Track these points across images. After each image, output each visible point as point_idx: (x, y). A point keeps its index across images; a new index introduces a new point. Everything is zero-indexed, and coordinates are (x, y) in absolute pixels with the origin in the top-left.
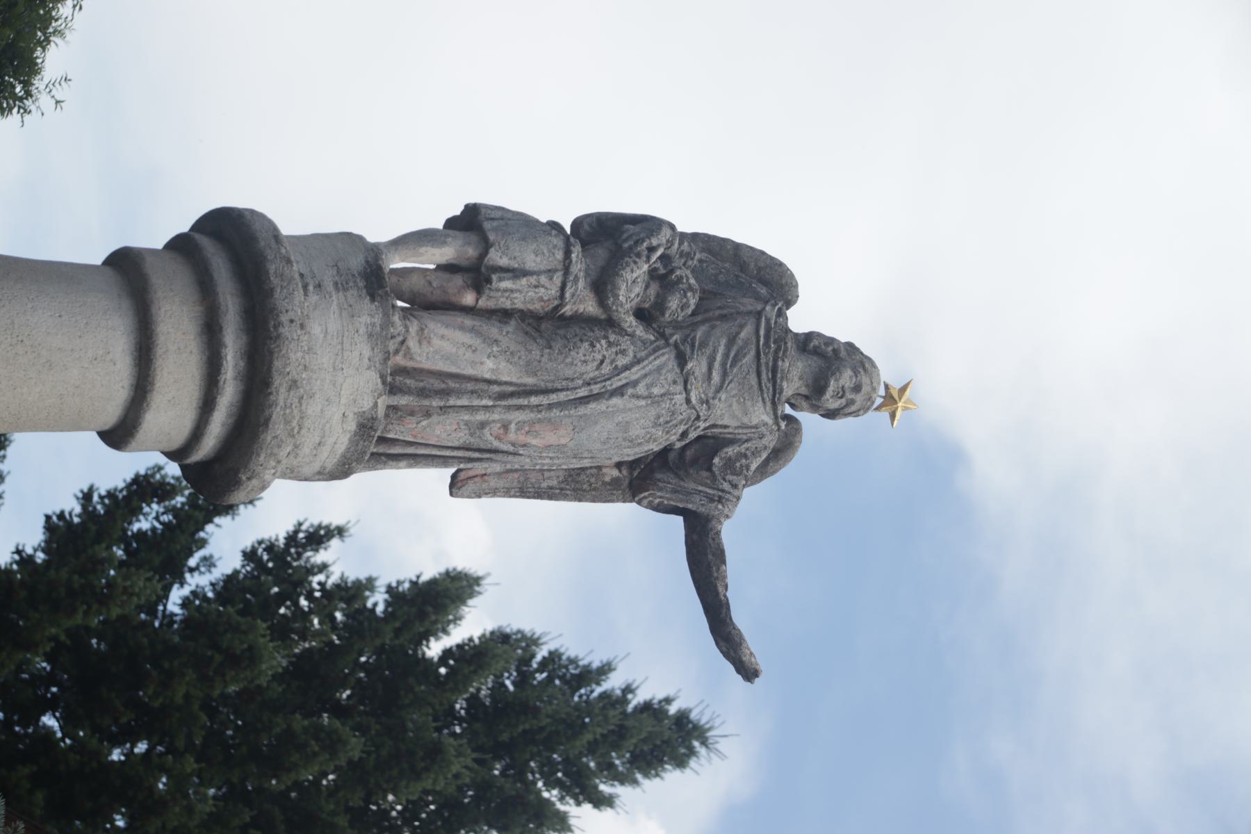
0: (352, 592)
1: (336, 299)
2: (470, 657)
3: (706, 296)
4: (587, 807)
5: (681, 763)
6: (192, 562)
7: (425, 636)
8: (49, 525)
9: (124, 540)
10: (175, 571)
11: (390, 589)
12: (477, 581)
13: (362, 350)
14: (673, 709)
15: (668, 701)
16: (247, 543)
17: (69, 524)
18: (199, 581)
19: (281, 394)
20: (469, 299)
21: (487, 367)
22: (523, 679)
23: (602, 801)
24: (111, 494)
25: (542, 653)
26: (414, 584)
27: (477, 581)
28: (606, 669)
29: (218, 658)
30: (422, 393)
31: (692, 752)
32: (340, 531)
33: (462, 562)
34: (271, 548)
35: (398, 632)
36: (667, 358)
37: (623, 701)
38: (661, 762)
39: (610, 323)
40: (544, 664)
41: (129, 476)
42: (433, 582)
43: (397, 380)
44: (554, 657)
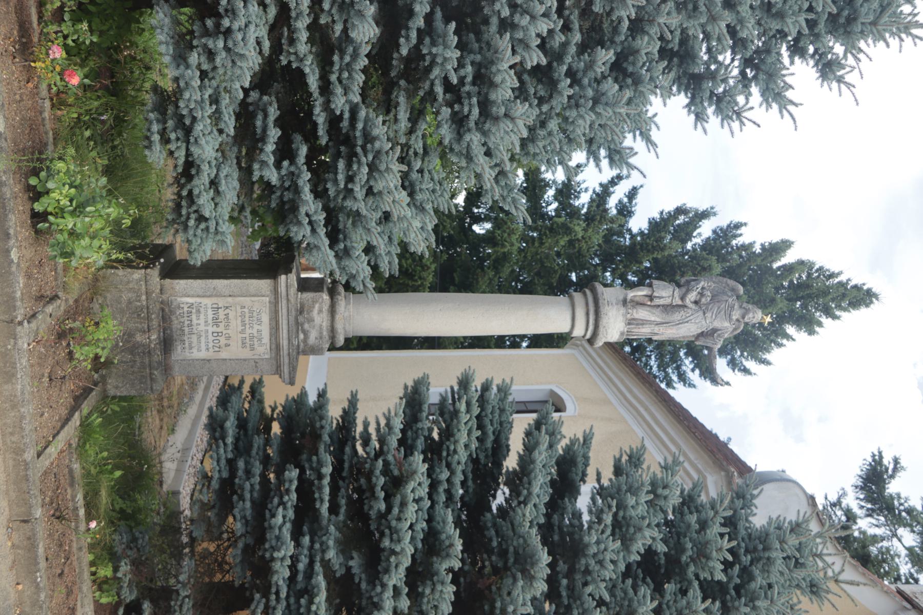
0: (747, 247)
1: (615, 307)
2: (789, 269)
3: (713, 297)
4: (830, 319)
5: (867, 306)
6: (694, 234)
7: (773, 261)
8: (650, 223)
9: (673, 226)
10: (689, 237)
11: (762, 245)
12: (793, 243)
13: (621, 318)
14: (865, 288)
15: (864, 284)
16: (713, 227)
17: (656, 222)
18: (697, 240)
19: (601, 329)
20: (649, 303)
21: (653, 319)
22: (809, 275)
23: (835, 317)
24: (669, 213)
25: (817, 267)
26: (770, 244)
27: (793, 243)
28: (839, 274)
29: (699, 268)
30: (637, 324)
31: (872, 302)
32: (745, 224)
33: (790, 238)
34: (721, 229)
35: (762, 260)
36: (701, 313)
37: (847, 283)
38: (860, 305)
39: (684, 306)
40: (817, 271)
41: (675, 207)
42: (777, 243)
43: (630, 322)
44: (821, 269)
